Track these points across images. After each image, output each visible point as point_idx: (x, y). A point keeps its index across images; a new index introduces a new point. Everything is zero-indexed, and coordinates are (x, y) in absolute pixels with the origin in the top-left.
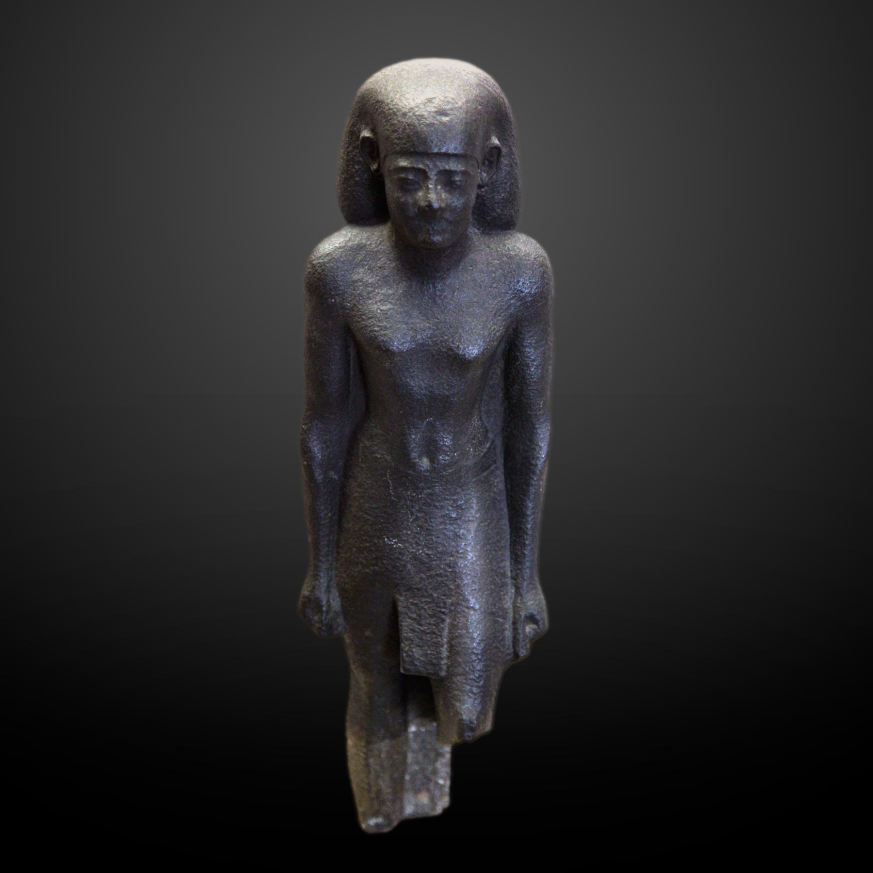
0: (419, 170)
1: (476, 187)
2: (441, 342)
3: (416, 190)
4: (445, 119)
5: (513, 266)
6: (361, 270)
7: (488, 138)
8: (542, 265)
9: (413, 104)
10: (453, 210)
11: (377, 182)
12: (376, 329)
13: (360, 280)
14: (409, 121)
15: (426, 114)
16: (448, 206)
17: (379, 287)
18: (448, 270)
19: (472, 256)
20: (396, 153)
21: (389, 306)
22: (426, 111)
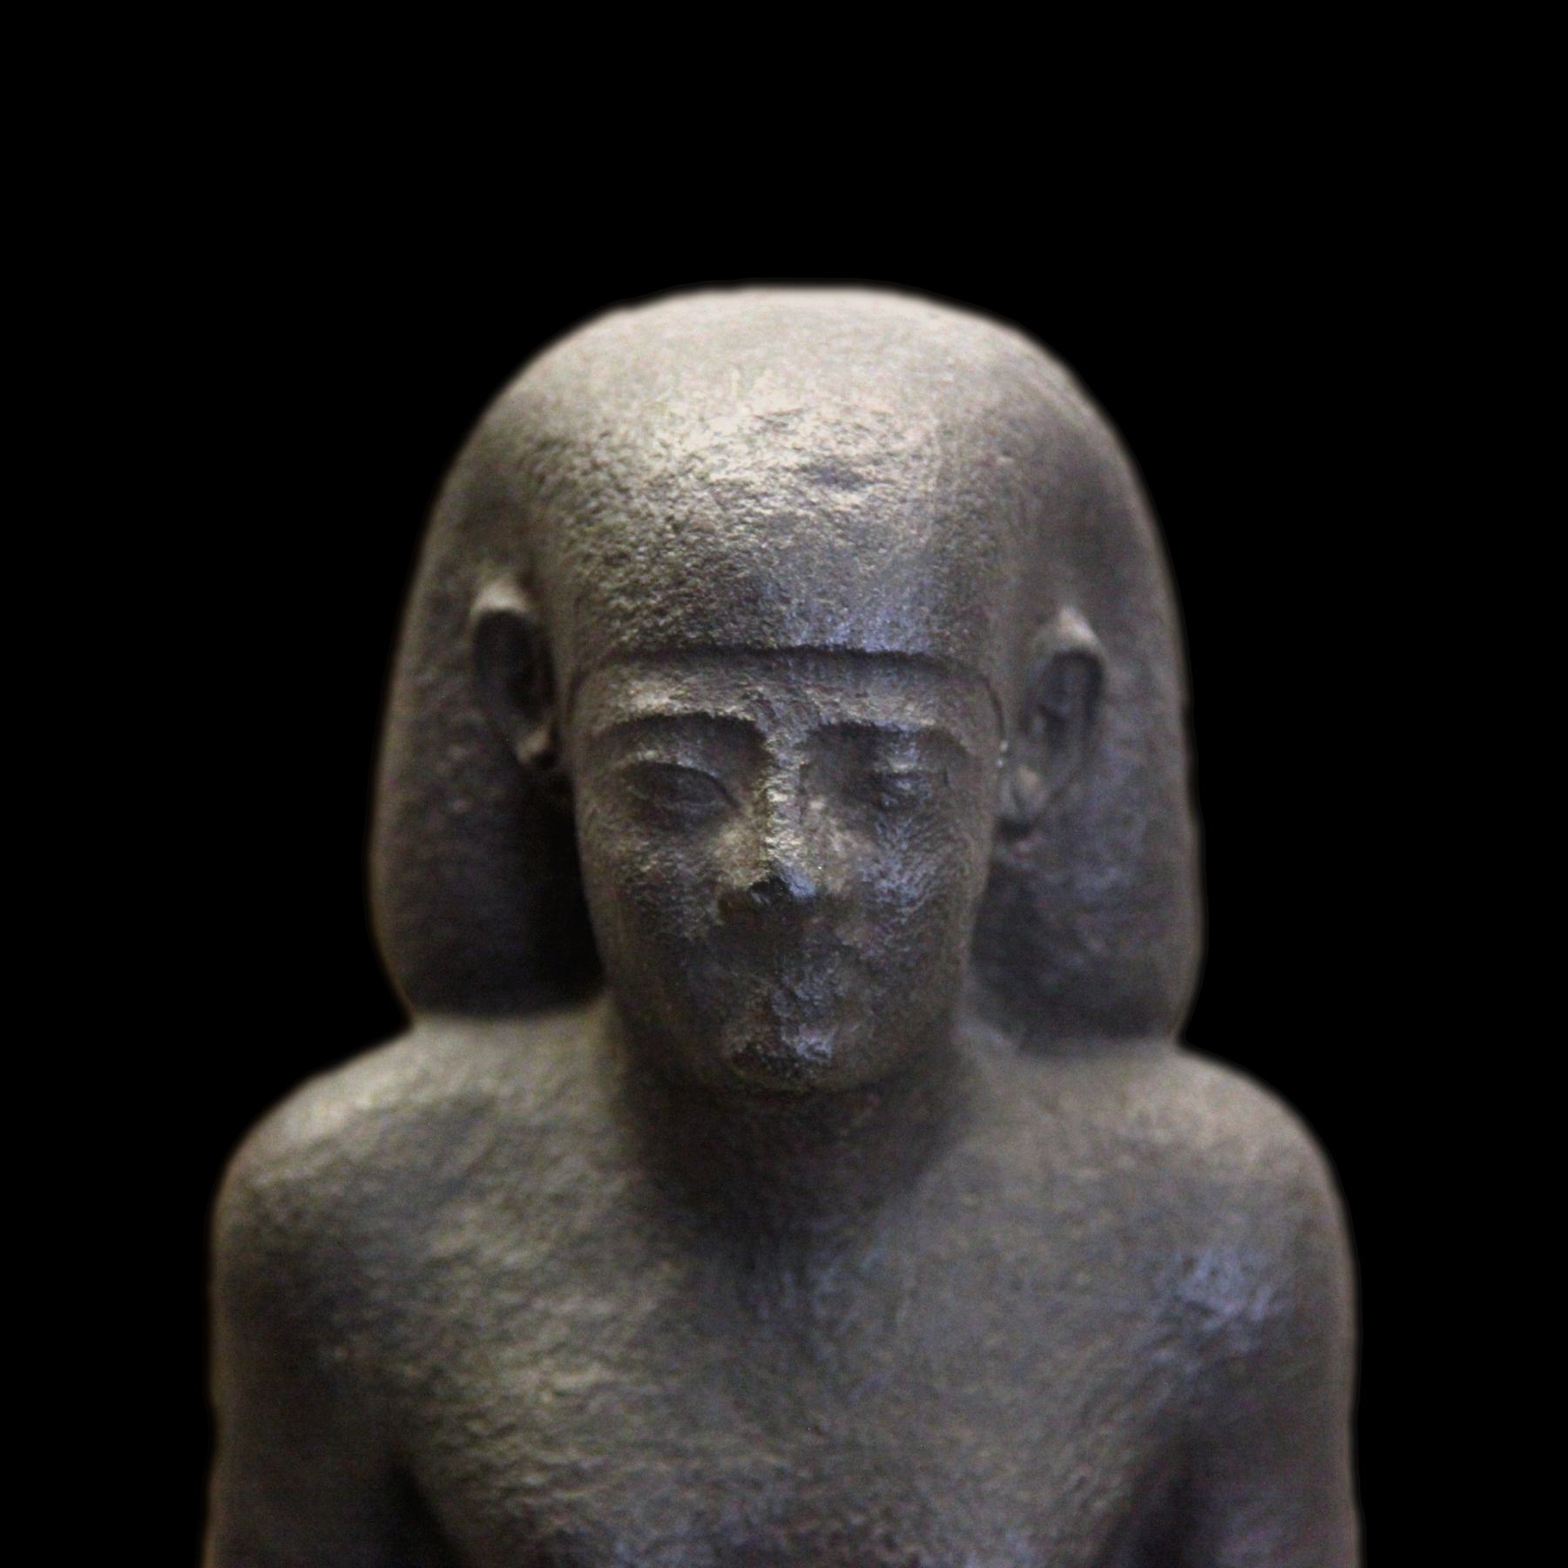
0: (728, 725)
1: (986, 828)
2: (835, 1538)
3: (713, 821)
4: (844, 500)
5: (1162, 1202)
6: (471, 1213)
7: (1045, 617)
8: (1297, 1192)
9: (697, 441)
10: (881, 912)
11: (541, 816)
12: (533, 1479)
13: (465, 1257)
14: (680, 512)
15: (757, 480)
16: (863, 890)
17: (553, 1286)
18: (869, 1204)
19: (971, 1146)
20: (625, 656)
21: (594, 1374)
22: (758, 466)
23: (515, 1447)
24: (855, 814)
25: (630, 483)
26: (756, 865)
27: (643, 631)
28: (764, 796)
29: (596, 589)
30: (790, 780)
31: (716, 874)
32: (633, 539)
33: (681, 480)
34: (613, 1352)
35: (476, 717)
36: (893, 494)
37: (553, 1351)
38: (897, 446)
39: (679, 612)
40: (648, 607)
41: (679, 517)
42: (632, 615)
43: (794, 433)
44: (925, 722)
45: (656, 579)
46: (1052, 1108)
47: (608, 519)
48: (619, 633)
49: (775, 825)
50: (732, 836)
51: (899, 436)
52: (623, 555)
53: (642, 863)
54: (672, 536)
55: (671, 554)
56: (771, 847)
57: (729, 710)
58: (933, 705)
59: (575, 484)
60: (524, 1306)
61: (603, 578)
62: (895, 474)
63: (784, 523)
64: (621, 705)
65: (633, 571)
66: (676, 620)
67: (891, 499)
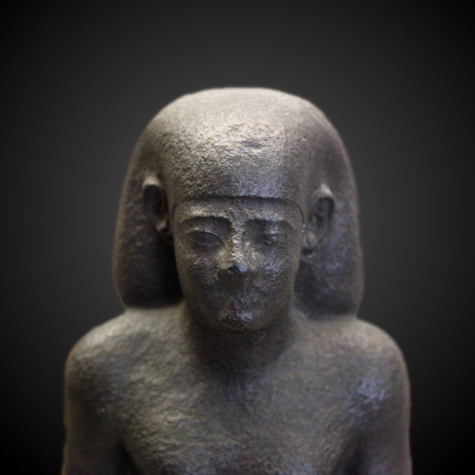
0: (221, 220)
1: (299, 251)
2: (253, 466)
3: (216, 249)
4: (256, 151)
5: (352, 364)
6: (143, 368)
7: (316, 187)
8: (393, 361)
9: (211, 134)
10: (267, 276)
11: (164, 247)
12: (161, 448)
13: (141, 381)
14: (206, 155)
15: (229, 145)
16: (261, 270)
17: (167, 390)
18: (263, 365)
19: (294, 347)
20: (189, 199)
21: (180, 416)
22: (230, 141)
23: (156, 438)
24: (259, 246)
25: (191, 146)
26: (229, 262)
27: (195, 191)
28: (231, 241)
29: (181, 179)
30: (239, 236)
31: (217, 265)
32: (192, 163)
33: (206, 145)
34: (186, 409)
35: (144, 217)
36: (270, 150)
37: (168, 409)
38: (272, 135)
39: (206, 185)
40: (196, 184)
41: (206, 157)
42: (192, 186)
43: (240, 131)
44: (280, 219)
45: (199, 175)
46: (319, 336)
47: (184, 157)
48: (188, 192)
49: (235, 250)
50: (222, 253)
51: (272, 132)
52: (189, 168)
53: (194, 261)
54: (204, 162)
55: (203, 168)
56: (234, 256)
57: (221, 215)
58: (283, 214)
59: (174, 146)
60: (159, 396)
61: (183, 175)
62: (271, 144)
63: (237, 158)
64: (188, 214)
65: (192, 173)
66: (205, 188)
67: (270, 151)
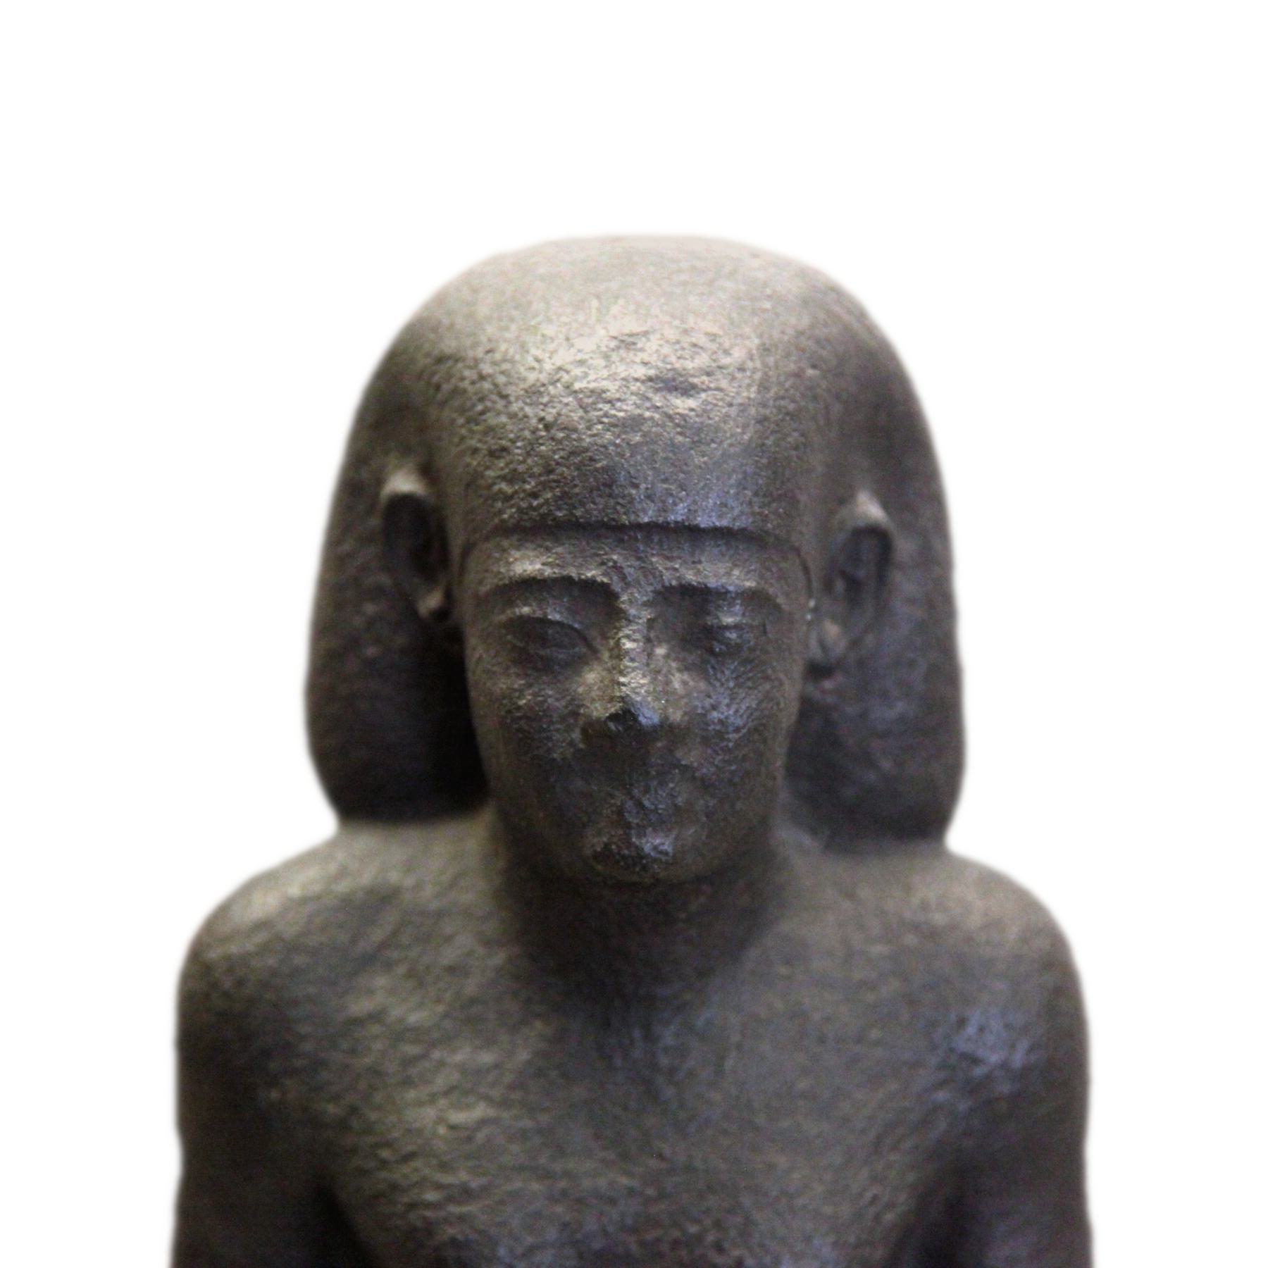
0: (589, 586)
1: (797, 669)
2: (676, 1244)
3: (576, 664)
4: (682, 404)
6: (381, 981)
7: (845, 499)
9: (563, 357)
10: (713, 737)
11: (437, 660)
12: (431, 1196)
13: (376, 1017)
14: (550, 414)
15: (612, 388)
16: (698, 720)
17: (447, 1040)
18: (703, 974)
19: (786, 927)
20: (505, 530)
21: (480, 1111)
22: (613, 377)
23: (416, 1170)
24: (691, 658)
25: (509, 390)
26: (612, 699)
27: (520, 510)
28: (618, 644)
29: (482, 477)
30: (638, 631)
31: (579, 706)
32: (512, 436)
33: (551, 388)
34: (496, 1093)
35: (385, 580)
36: (722, 400)
37: (447, 1093)
38: (725, 361)
39: (549, 495)
40: (524, 491)
41: (549, 418)
42: (511, 497)
43: (642, 350)
44: (748, 584)
45: (530, 468)
46: (851, 896)
47: (491, 419)
48: (501, 512)
49: (627, 667)
50: (592, 676)
51: (727, 352)
52: (504, 449)
53: (519, 698)
54: (543, 433)
55: (543, 448)
56: (624, 685)
57: (589, 575)
58: (755, 570)
59: (465, 391)
60: (424, 1056)
61: (488, 468)
62: (724, 384)
63: (634, 423)
64: (503, 570)
65: (511, 462)
66: (547, 502)
67: (720, 403)
